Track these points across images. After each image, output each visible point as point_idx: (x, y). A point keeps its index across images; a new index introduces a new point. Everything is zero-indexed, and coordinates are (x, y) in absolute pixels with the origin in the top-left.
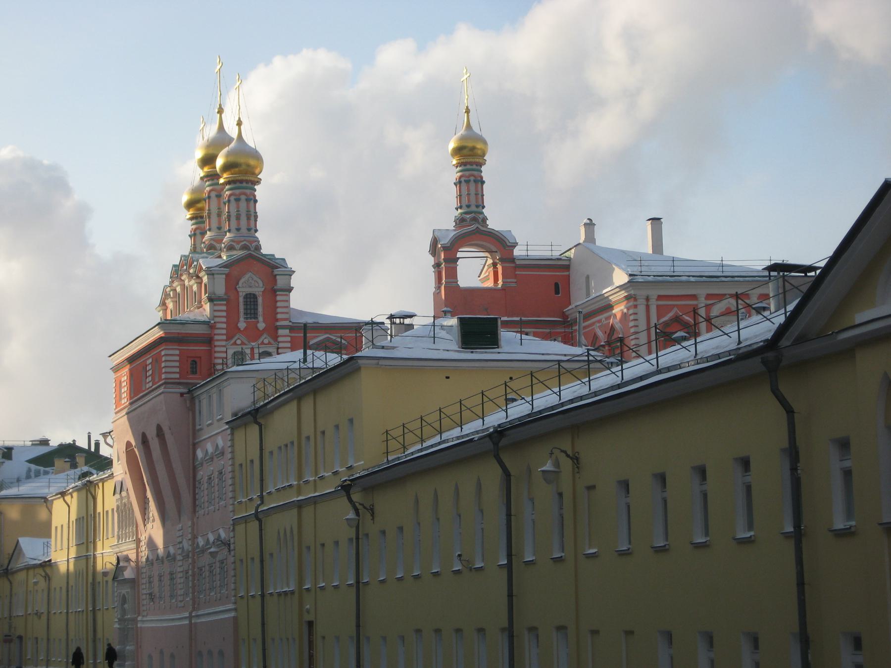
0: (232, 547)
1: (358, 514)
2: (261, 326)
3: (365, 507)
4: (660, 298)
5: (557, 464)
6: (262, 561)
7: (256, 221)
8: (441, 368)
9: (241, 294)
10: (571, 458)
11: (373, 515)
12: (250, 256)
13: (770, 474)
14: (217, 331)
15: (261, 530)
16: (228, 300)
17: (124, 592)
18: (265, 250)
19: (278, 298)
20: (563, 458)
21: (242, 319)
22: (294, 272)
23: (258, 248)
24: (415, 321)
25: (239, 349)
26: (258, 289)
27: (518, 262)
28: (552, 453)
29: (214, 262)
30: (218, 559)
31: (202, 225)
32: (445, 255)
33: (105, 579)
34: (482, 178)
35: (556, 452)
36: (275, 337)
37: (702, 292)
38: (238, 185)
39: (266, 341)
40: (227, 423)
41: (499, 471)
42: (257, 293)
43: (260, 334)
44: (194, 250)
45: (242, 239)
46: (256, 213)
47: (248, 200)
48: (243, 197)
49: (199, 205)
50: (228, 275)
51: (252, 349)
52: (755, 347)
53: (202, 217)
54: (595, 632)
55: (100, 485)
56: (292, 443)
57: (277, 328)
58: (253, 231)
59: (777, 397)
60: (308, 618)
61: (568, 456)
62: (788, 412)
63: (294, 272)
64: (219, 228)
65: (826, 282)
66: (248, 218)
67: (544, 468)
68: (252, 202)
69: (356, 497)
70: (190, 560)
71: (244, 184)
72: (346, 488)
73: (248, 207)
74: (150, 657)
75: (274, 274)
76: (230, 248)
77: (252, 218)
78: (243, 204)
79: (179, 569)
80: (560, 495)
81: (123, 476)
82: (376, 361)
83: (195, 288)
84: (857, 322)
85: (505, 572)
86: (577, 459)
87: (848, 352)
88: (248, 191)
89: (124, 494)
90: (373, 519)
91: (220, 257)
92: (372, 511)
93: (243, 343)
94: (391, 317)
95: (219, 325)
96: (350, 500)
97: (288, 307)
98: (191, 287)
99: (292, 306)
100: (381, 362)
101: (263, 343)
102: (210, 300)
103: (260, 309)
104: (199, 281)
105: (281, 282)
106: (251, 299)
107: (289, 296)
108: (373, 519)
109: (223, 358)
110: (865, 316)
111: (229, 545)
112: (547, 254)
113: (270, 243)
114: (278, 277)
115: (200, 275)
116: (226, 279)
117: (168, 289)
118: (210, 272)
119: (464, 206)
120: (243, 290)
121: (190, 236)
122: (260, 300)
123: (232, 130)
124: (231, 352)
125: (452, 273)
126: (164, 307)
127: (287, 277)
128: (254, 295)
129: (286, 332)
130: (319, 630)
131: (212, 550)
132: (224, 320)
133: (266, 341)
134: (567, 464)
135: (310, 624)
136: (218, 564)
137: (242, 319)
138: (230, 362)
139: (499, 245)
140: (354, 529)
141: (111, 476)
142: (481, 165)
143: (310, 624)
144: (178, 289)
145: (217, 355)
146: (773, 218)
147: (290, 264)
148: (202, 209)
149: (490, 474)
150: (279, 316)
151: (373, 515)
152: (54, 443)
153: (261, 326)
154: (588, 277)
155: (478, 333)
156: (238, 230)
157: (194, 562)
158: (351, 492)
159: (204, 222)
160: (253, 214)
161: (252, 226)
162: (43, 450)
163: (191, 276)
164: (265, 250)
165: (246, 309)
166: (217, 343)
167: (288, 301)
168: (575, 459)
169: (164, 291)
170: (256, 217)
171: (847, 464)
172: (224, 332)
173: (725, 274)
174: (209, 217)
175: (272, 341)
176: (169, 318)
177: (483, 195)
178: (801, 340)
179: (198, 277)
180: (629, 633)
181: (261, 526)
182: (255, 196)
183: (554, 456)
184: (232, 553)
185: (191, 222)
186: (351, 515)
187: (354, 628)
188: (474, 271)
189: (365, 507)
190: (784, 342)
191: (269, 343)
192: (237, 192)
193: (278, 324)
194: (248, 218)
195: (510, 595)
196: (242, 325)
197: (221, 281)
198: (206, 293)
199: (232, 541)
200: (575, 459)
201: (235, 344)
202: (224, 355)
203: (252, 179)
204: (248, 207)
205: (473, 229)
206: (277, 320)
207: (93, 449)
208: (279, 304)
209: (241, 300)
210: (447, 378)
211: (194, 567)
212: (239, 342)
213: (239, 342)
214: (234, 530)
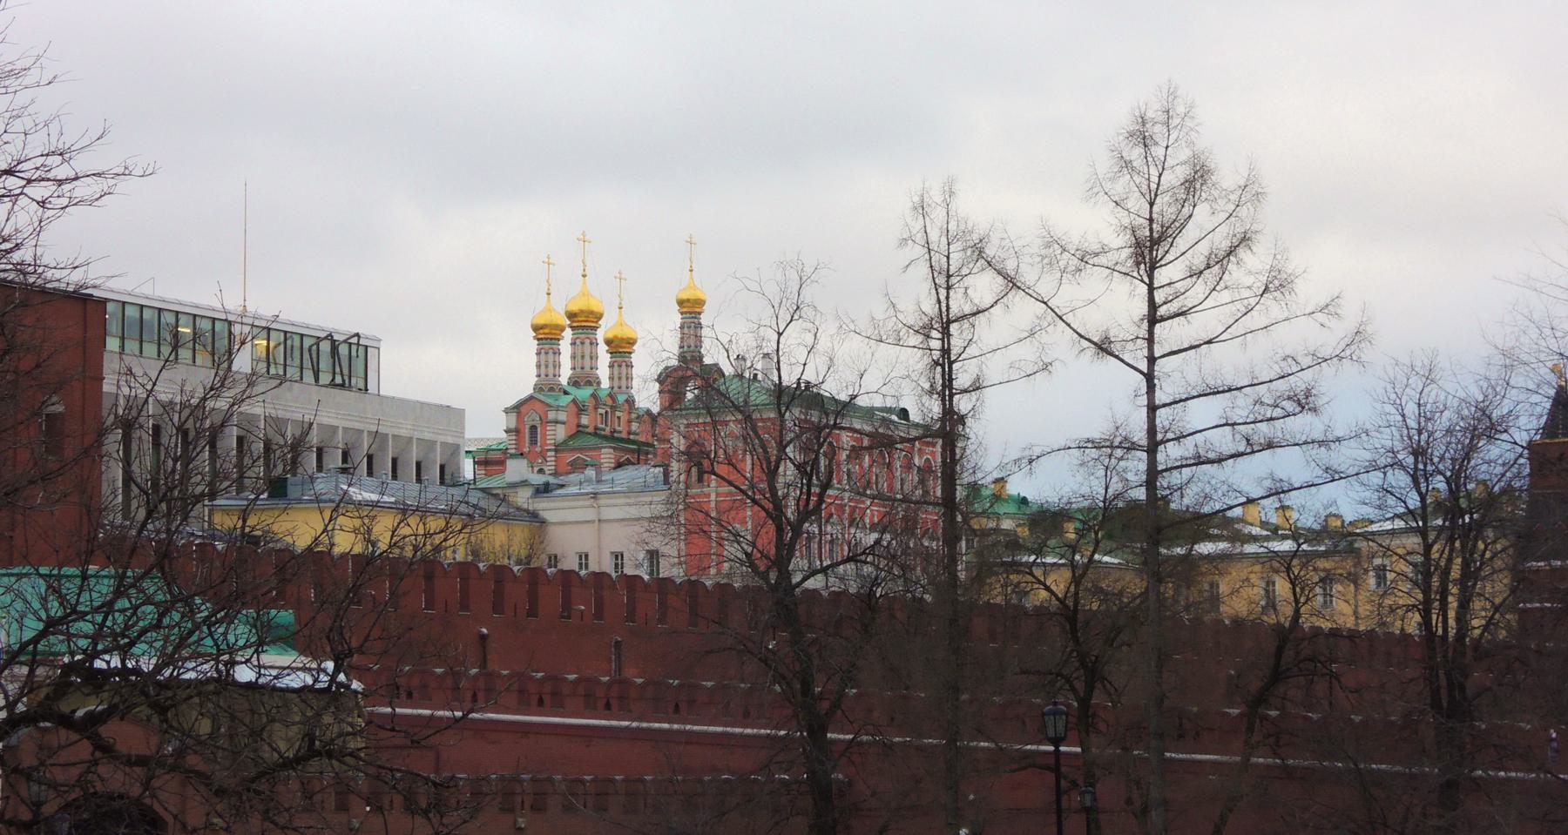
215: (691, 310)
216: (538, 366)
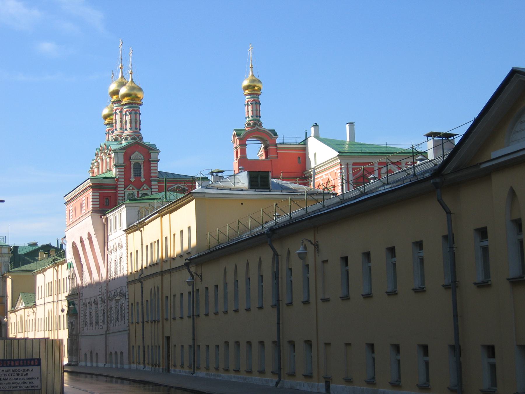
0: (127, 297)
1: (193, 278)
2: (143, 180)
3: (197, 275)
4: (354, 164)
5: (305, 248)
6: (142, 304)
7: (140, 124)
8: (240, 200)
9: (132, 163)
10: (314, 245)
11: (201, 279)
13: (435, 252)
14: (119, 183)
15: (142, 288)
17: (72, 320)
19: (152, 165)
20: (308, 244)
21: (132, 176)
23: (141, 139)
24: (224, 174)
25: (130, 192)
26: (141, 161)
27: (279, 146)
28: (303, 242)
29: (118, 147)
30: (120, 303)
32: (243, 138)
33: (63, 314)
34: (259, 102)
35: (306, 242)
36: (150, 186)
37: (376, 161)
38: (131, 105)
39: (145, 188)
40: (124, 231)
41: (272, 253)
43: (142, 184)
46: (140, 120)
47: (136, 113)
48: (133, 112)
49: (111, 117)
51: (138, 192)
53: (112, 123)
54: (327, 344)
56: (158, 241)
57: (151, 181)
60: (167, 334)
61: (312, 243)
62: (447, 213)
64: (121, 129)
65: (473, 132)
66: (136, 122)
67: (299, 251)
68: (138, 115)
69: (193, 269)
70: (106, 304)
71: (134, 105)
72: (187, 265)
74: (86, 355)
75: (149, 152)
76: (126, 139)
77: (138, 123)
79: (100, 309)
80: (307, 266)
81: (71, 260)
82: (203, 195)
83: (108, 160)
84: (492, 158)
86: (317, 245)
87: (486, 175)
88: (136, 109)
89: (72, 269)
90: (201, 281)
91: (121, 144)
92: (201, 276)
93: (133, 189)
94: (212, 173)
96: (189, 271)
97: (157, 170)
98: (106, 159)
100: (206, 195)
101: (143, 189)
102: (116, 166)
104: (110, 156)
105: (153, 156)
108: (201, 281)
109: (122, 197)
110: (498, 152)
111: (126, 296)
112: (293, 142)
114: (151, 154)
115: (111, 153)
118: (116, 151)
119: (250, 116)
120: (133, 162)
122: (142, 166)
124: (126, 194)
125: (243, 152)
129: (156, 183)
130: (173, 342)
131: (117, 298)
133: (145, 188)
134: (311, 248)
135: (168, 338)
136: (120, 306)
137: (132, 176)
138: (126, 198)
139: (268, 138)
140: (191, 287)
141: (65, 262)
142: (259, 95)
143: (168, 338)
144: (99, 161)
145: (119, 195)
146: (423, 111)
148: (112, 119)
149: (55, 303)
150: (152, 175)
151: (201, 279)
152: (40, 244)
153: (143, 180)
154: (315, 154)
155: (259, 179)
157: (108, 305)
158: (190, 266)
159: (113, 126)
161: (138, 127)
162: (34, 248)
163: (106, 154)
165: (134, 173)
166: (119, 189)
167: (157, 167)
168: (316, 246)
171: (484, 244)
172: (123, 183)
173: (388, 151)
174: (116, 124)
175: (149, 188)
176: (95, 175)
177: (260, 111)
178: (457, 170)
179: (109, 154)
180: (348, 345)
181: (142, 285)
182: (139, 111)
183: (304, 244)
184: (127, 300)
186: (189, 279)
187: (192, 341)
188: (256, 152)
189: (197, 275)
190: (448, 169)
191: (147, 189)
193: (152, 179)
194: (136, 122)
195: (279, 323)
196: (133, 180)
197: (122, 155)
199: (127, 294)
200: (316, 246)
201: (129, 189)
202: (123, 195)
203: (138, 102)
205: (256, 131)
206: (151, 177)
207: (59, 247)
208: (152, 168)
209: (132, 166)
210: (242, 204)
211: (107, 308)
212: (131, 188)
213: (131, 188)
214: (128, 288)
215: (254, 91)
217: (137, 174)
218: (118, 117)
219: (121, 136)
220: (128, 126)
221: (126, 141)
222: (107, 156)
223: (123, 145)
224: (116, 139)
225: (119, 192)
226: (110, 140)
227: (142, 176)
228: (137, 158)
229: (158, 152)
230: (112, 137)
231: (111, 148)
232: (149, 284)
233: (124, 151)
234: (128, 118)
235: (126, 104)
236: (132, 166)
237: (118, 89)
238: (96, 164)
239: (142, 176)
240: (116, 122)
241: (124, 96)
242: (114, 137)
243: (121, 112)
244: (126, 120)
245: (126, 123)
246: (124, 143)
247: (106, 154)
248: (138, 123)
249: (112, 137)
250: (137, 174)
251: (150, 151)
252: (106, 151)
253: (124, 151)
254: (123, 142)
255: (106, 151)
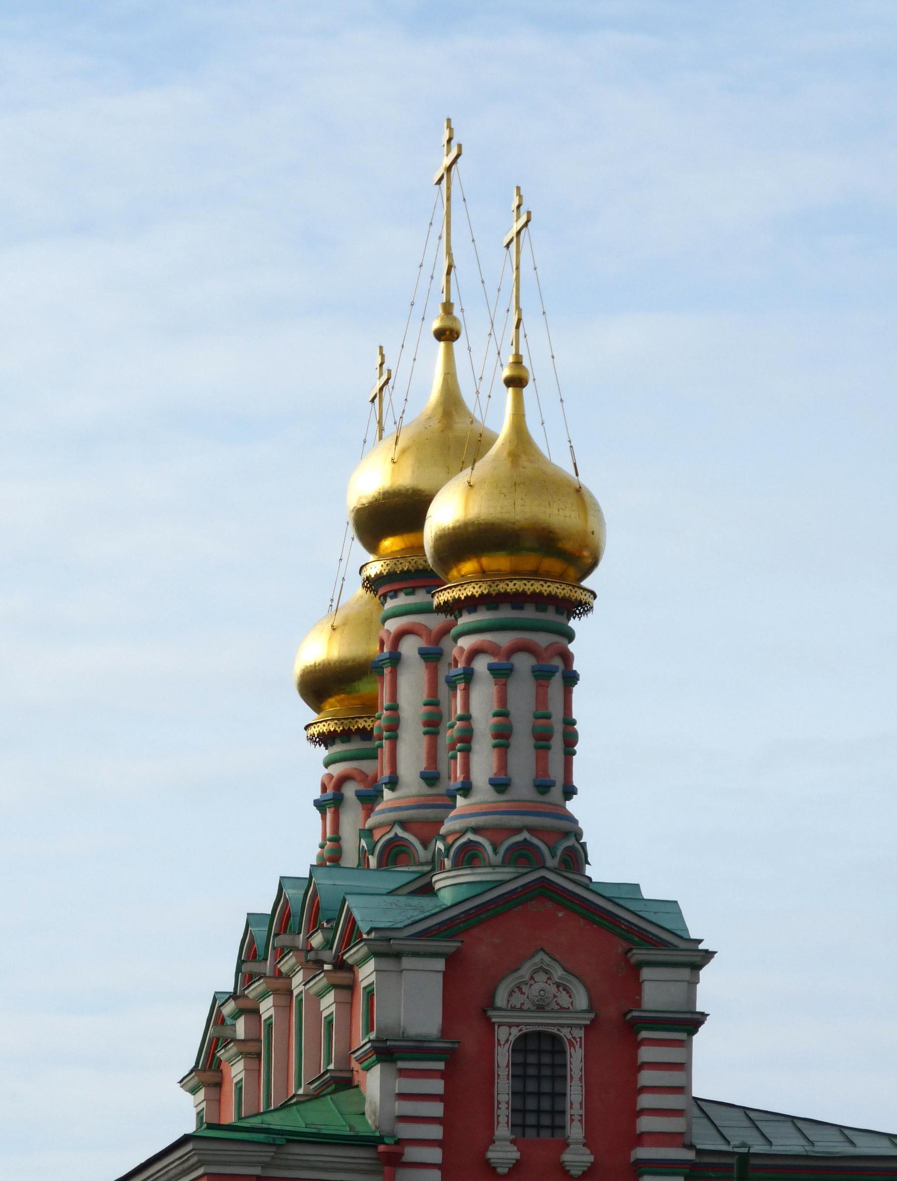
9: (502, 1034)
12: (544, 889)
16: (451, 1057)
18: (602, 868)
19: (647, 1054)
21: (503, 1131)
22: (708, 955)
23: (575, 857)
31: (366, 766)
38: (505, 613)
42: (565, 1033)
44: (332, 856)
45: (516, 821)
46: (569, 722)
47: (542, 675)
48: (524, 663)
49: (365, 688)
50: (452, 960)
52: (865, 1147)
55: (387, 671)
58: (556, 793)
59: (412, 1117)
63: (708, 955)
64: (430, 778)
66: (542, 739)
68: (557, 682)
73: (541, 700)
75: (638, 960)
76: (468, 856)
77: (557, 743)
78: (522, 693)
83: (328, 1003)
85: (255, 1112)
88: (542, 640)
91: (428, 890)
95: (413, 1154)
97: (683, 1089)
99: (699, 1090)
103: (575, 1093)
104: (342, 977)
105: (657, 992)
106: (540, 1052)
107: (686, 1045)
113: (624, 838)
114: (646, 973)
116: (446, 975)
117: (229, 1008)
121: (320, 805)
122: (576, 1059)
123: (495, 414)
126: (210, 1076)
127: (685, 973)
128: (555, 1039)
132: (436, 1132)
137: (503, 1131)
147: (698, 926)
156: (500, 785)
160: (558, 728)
161: (556, 772)
164: (602, 868)
167: (684, 1067)
169: (216, 1018)
170: (570, 741)
174: (394, 740)
176: (230, 1117)
179: (340, 965)
182: (567, 658)
185: (322, 753)
192: (504, 639)
193: (643, 1153)
198: (369, 1027)
204: (541, 700)
206: (640, 1139)
209: (503, 1057)
216: (556, 737)
217: (538, 1112)
218: (411, 689)
219: (428, 830)
220: (483, 763)
221: (467, 876)
222: (321, 981)
223: (447, 897)
224: (393, 854)
225: (436, 1132)
226: (350, 858)
227: (575, 1131)
228: (547, 991)
229: (696, 958)
230: (367, 833)
231: (351, 922)
232: (557, 662)
233: (451, 946)
234: (482, 700)
235: (470, 604)
236: (503, 1057)
237: (424, 485)
238: (240, 1028)
239: (575, 1131)
240: (394, 727)
241: (462, 543)
242: (382, 838)
243: (432, 656)
244: (466, 718)
245: (466, 739)
246: (449, 886)
247: (319, 963)
248: (557, 743)
249: (367, 833)
250: (538, 1112)
251: (638, 955)
252: (317, 940)
253: (451, 946)
254: (440, 881)
255: (317, 940)
